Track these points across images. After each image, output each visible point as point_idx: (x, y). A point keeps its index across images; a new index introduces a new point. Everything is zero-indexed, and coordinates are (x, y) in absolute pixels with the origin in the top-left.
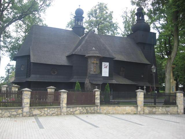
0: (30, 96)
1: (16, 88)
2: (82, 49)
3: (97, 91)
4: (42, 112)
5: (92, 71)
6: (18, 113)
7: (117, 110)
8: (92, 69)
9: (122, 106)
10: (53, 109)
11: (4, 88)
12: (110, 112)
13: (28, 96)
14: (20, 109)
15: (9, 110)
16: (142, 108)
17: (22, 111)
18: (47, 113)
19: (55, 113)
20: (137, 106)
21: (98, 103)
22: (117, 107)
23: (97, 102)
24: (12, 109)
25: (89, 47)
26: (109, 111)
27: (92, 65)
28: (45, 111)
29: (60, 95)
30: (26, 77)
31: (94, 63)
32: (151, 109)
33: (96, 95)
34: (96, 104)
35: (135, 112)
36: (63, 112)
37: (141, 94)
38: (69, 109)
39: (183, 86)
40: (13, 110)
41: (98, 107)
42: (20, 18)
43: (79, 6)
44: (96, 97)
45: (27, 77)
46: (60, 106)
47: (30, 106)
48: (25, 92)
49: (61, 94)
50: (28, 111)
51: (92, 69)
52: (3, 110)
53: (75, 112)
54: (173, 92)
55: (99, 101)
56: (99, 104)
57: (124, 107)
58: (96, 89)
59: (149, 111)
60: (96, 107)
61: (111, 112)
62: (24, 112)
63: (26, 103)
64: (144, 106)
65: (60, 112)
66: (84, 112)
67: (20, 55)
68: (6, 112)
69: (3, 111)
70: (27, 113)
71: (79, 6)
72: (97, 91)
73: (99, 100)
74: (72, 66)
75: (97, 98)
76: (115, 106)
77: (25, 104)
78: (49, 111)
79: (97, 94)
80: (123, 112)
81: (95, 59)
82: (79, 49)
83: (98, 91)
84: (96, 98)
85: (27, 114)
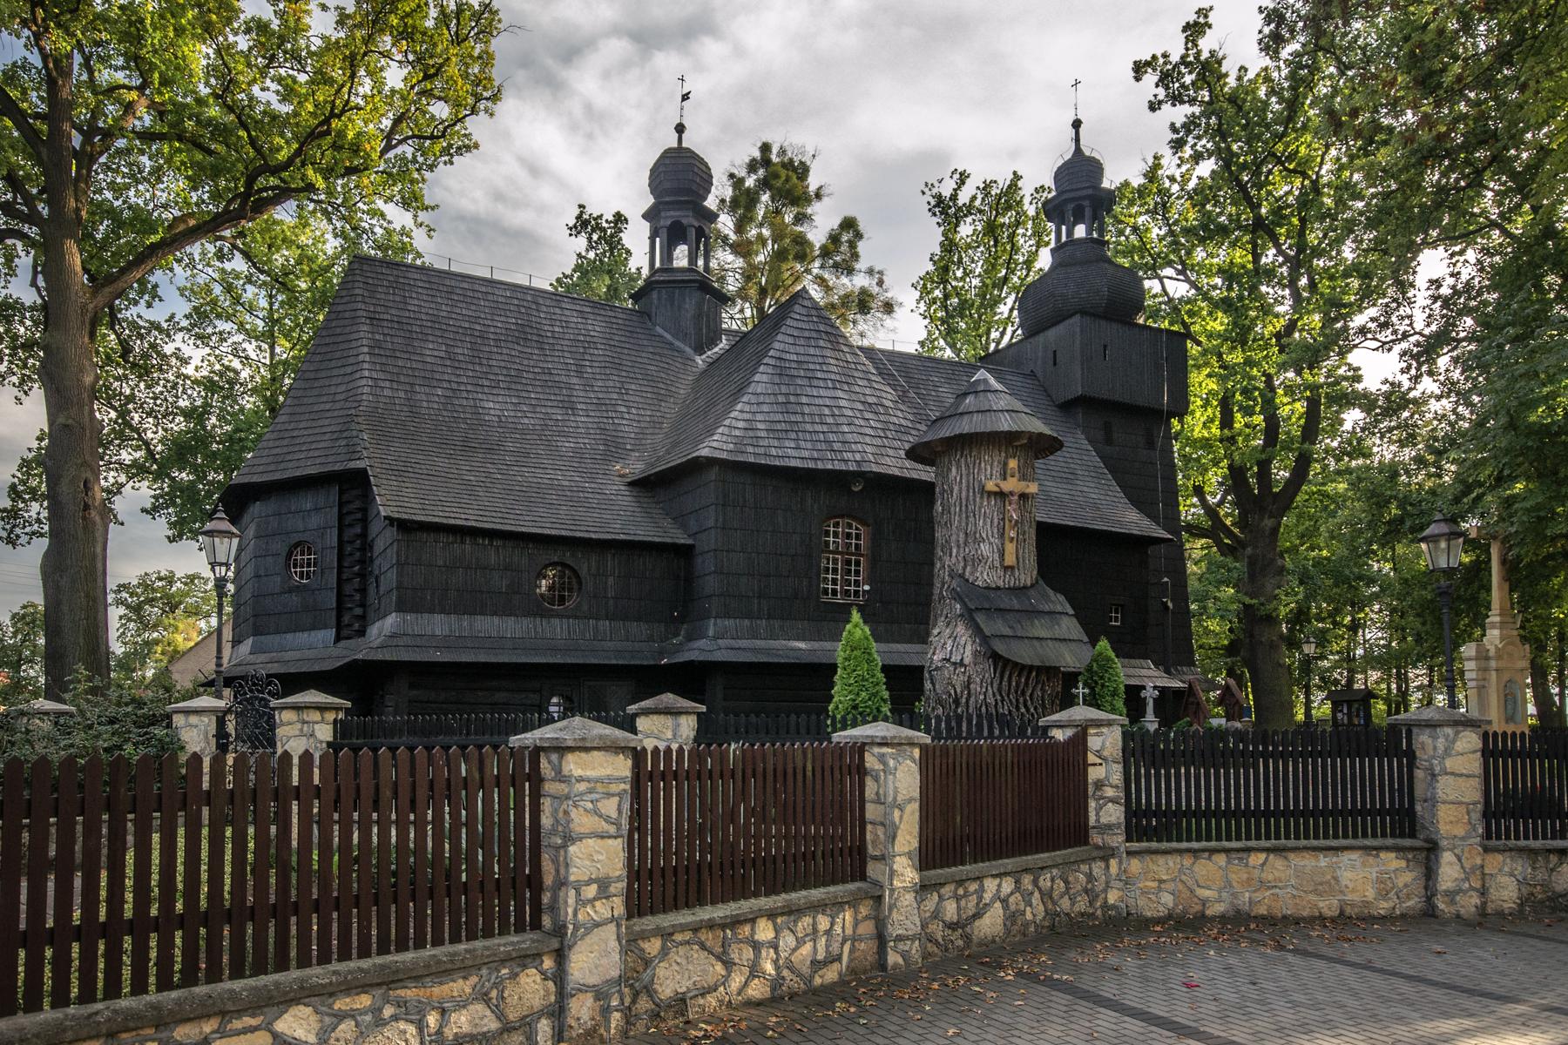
0: (626, 806)
1: (316, 716)
2: (763, 434)
3: (1098, 724)
4: (728, 964)
5: (981, 560)
6: (512, 1016)
7: (1263, 885)
8: (985, 549)
9: (1306, 848)
10: (823, 922)
11: (193, 719)
12: (1204, 902)
13: (610, 807)
14: (525, 959)
15: (409, 993)
16: (1467, 866)
17: (559, 977)
18: (769, 968)
19: (839, 958)
20: (1432, 849)
21: (1109, 827)
22: (1263, 856)
23: (1104, 820)
24: (443, 972)
25: (807, 410)
26: (1206, 893)
27: (989, 507)
28: (756, 946)
29: (861, 771)
30: (331, 633)
31: (1001, 495)
32: (1541, 875)
33: (1091, 758)
34: (1096, 839)
35: (1408, 897)
36: (899, 938)
37: (1460, 745)
38: (931, 902)
39: (555, 700)
40: (460, 987)
41: (1113, 863)
42: (208, 227)
43: (680, 129)
44: (1094, 774)
45: (338, 639)
46: (863, 877)
47: (638, 905)
48: (574, 765)
49: (871, 761)
50: (615, 973)
51: (985, 549)
52: (341, 1004)
53: (977, 923)
54: (1510, 729)
55: (1114, 814)
56: (1117, 840)
57: (1323, 861)
58: (1080, 712)
59: (1525, 891)
60: (1097, 868)
61: (1219, 901)
62: (583, 989)
63: (591, 891)
64: (1486, 850)
65: (873, 945)
66: (1029, 916)
67: (277, 476)
68: (380, 1023)
69: (341, 1016)
70: (600, 994)
71: (680, 129)
72: (1098, 724)
73: (1113, 801)
74: (692, 547)
75: (1099, 785)
76: (1249, 850)
77: (581, 902)
78: (788, 941)
79: (1098, 754)
80: (1312, 897)
81: (1013, 463)
82: (741, 424)
83: (1109, 724)
84: (1091, 790)
85: (606, 1011)
